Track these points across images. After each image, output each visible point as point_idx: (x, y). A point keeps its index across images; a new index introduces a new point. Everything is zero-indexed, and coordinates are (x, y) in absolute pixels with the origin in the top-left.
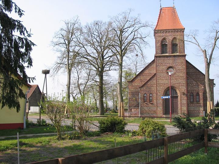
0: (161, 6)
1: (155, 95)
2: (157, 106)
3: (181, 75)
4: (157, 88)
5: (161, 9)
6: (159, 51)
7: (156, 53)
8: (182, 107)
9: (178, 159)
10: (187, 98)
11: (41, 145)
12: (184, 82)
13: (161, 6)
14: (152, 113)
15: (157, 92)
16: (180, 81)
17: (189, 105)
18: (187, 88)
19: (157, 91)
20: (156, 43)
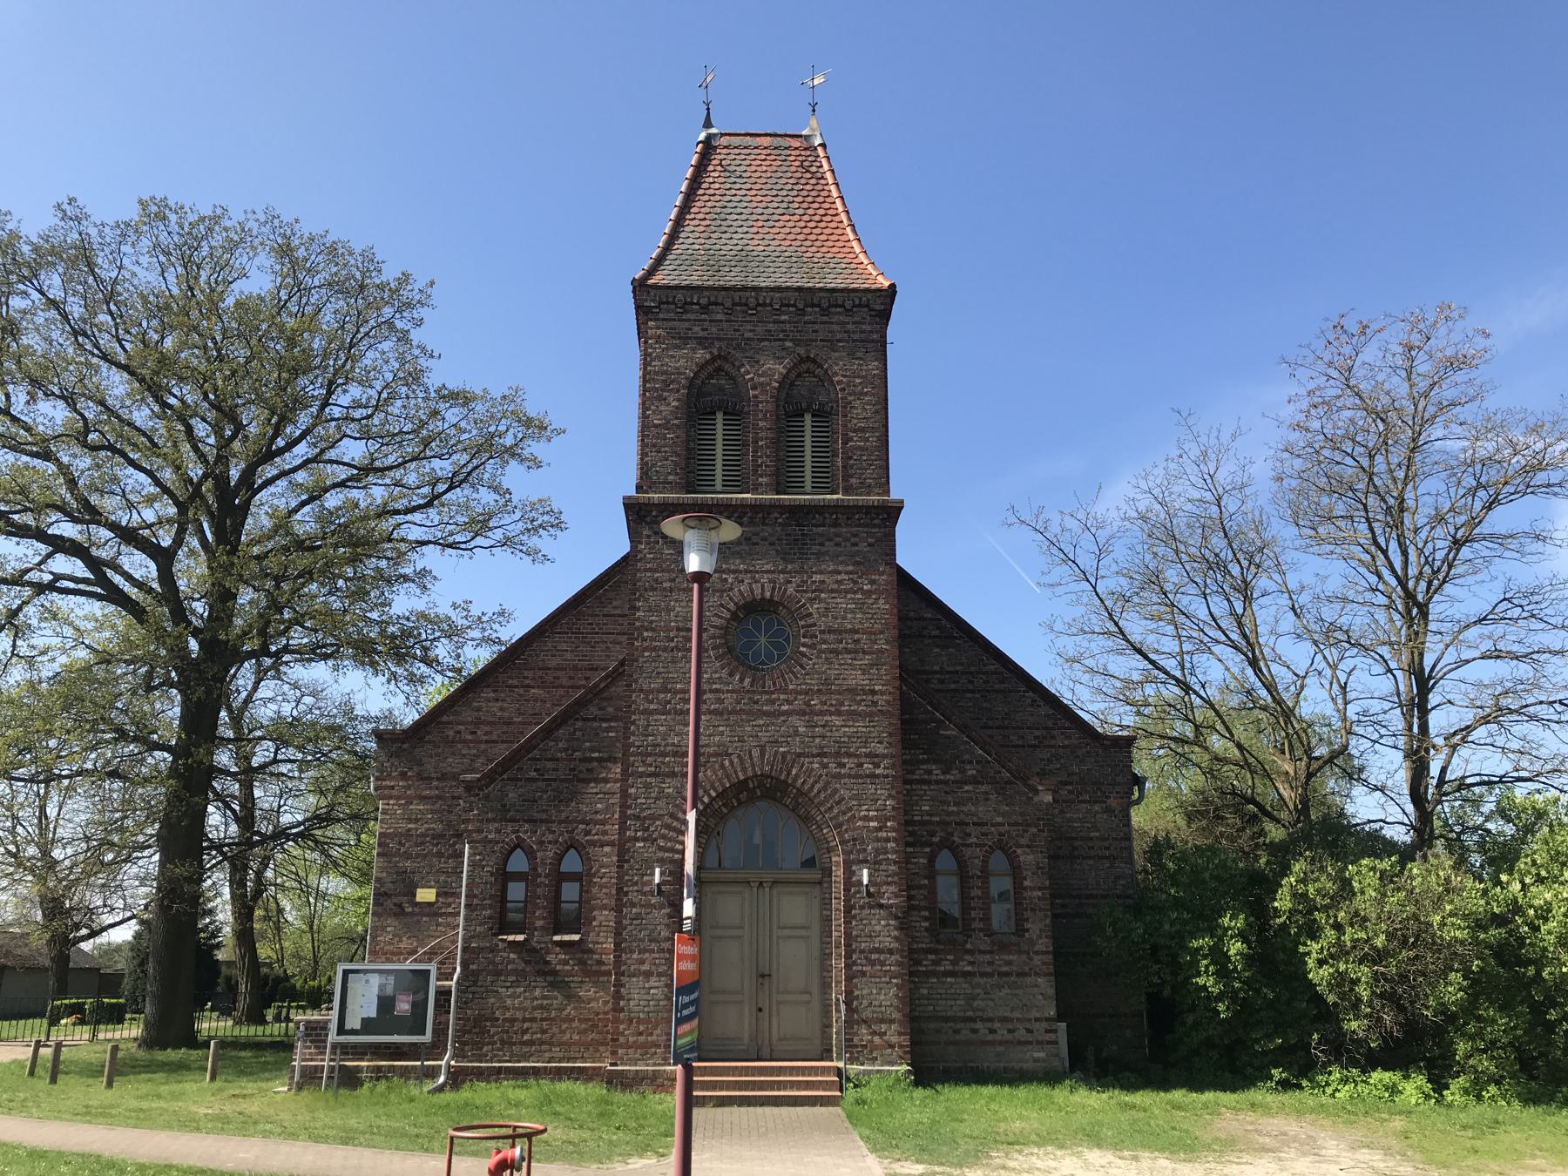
0: (708, 124)
1: (607, 856)
2: (620, 974)
3: (856, 678)
4: (624, 794)
5: (708, 147)
6: (666, 467)
7: (646, 480)
8: (863, 989)
9: (141, 1026)
10: (910, 898)
11: (691, 900)
12: (879, 738)
13: (708, 124)
14: (569, 1044)
15: (623, 828)
16: (841, 728)
17: (928, 960)
18: (906, 806)
19: (624, 818)
20: (652, 387)
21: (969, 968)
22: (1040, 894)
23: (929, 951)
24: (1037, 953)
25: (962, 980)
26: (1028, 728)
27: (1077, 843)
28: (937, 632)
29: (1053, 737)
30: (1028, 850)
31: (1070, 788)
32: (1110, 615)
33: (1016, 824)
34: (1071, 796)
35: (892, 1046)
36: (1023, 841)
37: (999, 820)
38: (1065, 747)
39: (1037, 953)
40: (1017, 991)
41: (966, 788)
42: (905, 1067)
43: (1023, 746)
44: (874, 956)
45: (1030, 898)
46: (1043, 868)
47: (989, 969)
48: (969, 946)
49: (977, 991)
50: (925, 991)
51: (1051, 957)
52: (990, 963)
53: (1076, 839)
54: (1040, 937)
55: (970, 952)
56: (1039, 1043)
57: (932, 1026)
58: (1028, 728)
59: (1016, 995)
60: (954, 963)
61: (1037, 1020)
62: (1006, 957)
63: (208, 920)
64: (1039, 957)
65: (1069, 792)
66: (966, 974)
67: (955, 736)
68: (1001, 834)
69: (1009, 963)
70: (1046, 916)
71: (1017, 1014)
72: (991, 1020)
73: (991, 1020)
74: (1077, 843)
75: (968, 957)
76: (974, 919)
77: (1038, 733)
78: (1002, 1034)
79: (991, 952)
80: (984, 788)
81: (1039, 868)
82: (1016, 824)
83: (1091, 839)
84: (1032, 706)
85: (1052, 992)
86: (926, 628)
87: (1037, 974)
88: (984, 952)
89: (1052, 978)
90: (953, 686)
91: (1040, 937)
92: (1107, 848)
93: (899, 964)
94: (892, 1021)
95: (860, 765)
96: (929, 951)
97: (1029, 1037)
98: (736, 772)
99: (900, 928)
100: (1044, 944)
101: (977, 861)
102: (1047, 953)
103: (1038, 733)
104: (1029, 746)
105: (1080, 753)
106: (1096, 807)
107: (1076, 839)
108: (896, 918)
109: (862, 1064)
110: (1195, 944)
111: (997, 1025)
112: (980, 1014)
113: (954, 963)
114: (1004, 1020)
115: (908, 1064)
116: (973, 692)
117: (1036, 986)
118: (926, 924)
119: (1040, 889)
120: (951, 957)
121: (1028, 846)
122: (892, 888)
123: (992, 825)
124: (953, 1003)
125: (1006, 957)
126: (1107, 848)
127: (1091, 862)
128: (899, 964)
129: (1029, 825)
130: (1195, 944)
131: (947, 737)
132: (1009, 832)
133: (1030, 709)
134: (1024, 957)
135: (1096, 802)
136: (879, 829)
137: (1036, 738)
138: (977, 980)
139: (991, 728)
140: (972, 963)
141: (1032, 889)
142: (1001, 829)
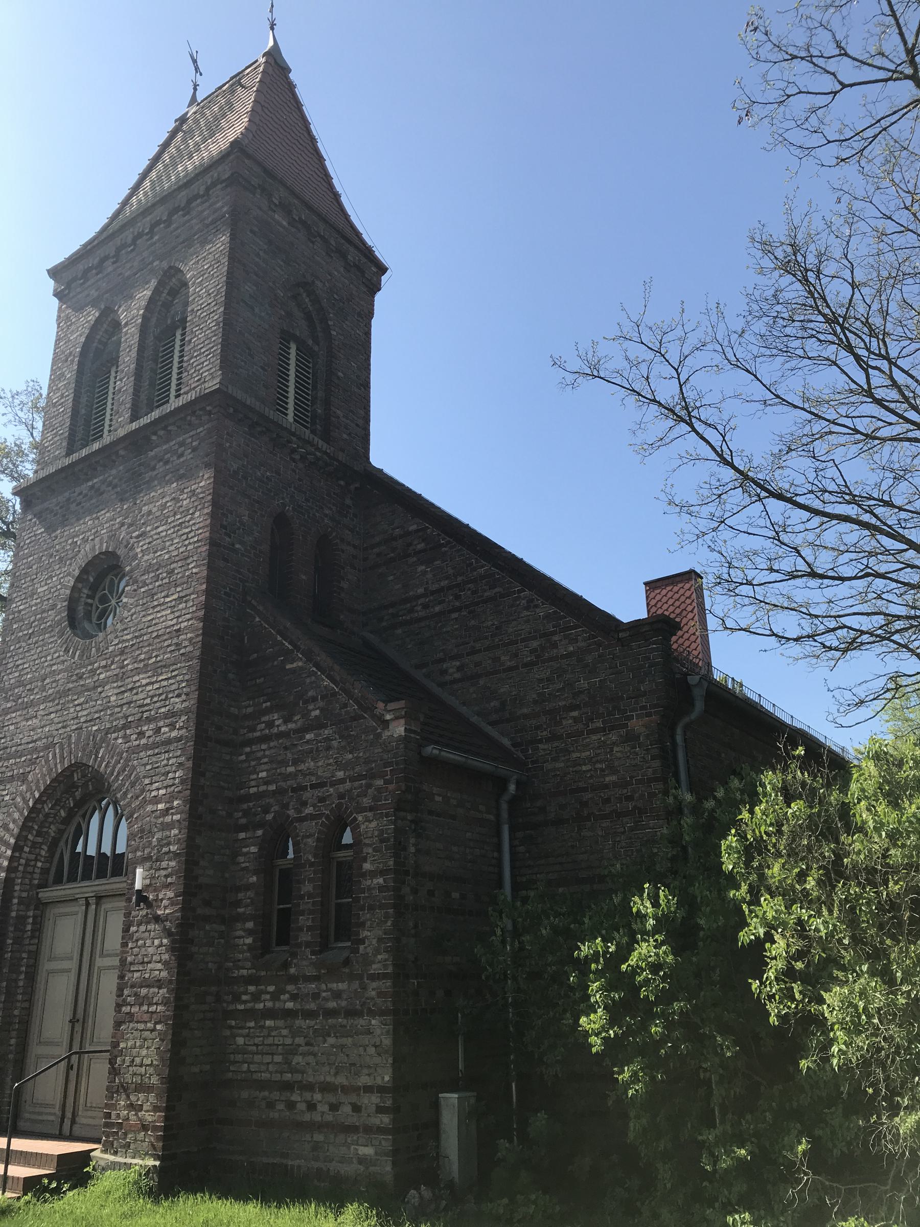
21: (290, 1005)
22: (381, 880)
23: (250, 980)
24: (373, 977)
25: (280, 1023)
26: (523, 640)
27: (587, 796)
28: (421, 546)
29: (554, 645)
30: (370, 814)
31: (575, 714)
32: (720, 456)
33: (360, 777)
34: (580, 726)
35: (145, 1128)
36: (366, 801)
37: (340, 774)
38: (569, 655)
39: (373, 977)
40: (344, 1041)
41: (308, 737)
42: (151, 1162)
43: (516, 668)
44: (144, 991)
45: (370, 889)
46: (387, 840)
47: (313, 1006)
48: (292, 971)
49: (298, 1040)
50: (240, 1041)
51: (389, 983)
52: (316, 996)
53: (585, 790)
54: (377, 951)
55: (294, 979)
56: (368, 1130)
57: (245, 1094)
58: (523, 640)
59: (342, 1046)
60: (275, 997)
61: (368, 1089)
62: (334, 986)
63: (915, 992)
64: (374, 984)
65: (575, 719)
66: (289, 1014)
67: (301, 668)
68: (341, 796)
69: (337, 995)
70: (387, 916)
71: (341, 1080)
72: (310, 1087)
73: (310, 1087)
74: (587, 796)
75: (290, 988)
76: (301, 929)
77: (535, 644)
78: (322, 1112)
79: (317, 978)
80: (327, 732)
81: (382, 841)
82: (360, 777)
83: (606, 786)
84: (527, 608)
85: (387, 1042)
86: (410, 544)
87: (372, 1013)
88: (308, 979)
89: (389, 1019)
90: (437, 609)
91: (377, 951)
92: (629, 798)
93: (165, 1002)
94: (148, 1089)
95: (158, 730)
96: (250, 980)
97: (354, 1120)
98: (56, 765)
99: (172, 949)
100: (381, 963)
101: (310, 841)
102: (385, 976)
103: (535, 644)
104: (526, 665)
105: (589, 659)
106: (613, 737)
107: (585, 790)
108: (169, 934)
109: (115, 1153)
110: (585, 950)
111: (318, 1096)
112: (298, 1077)
113: (275, 997)
114: (326, 1088)
115: (156, 1157)
116: (459, 609)
117: (369, 1032)
118: (249, 941)
119: (382, 873)
120: (271, 988)
121: (371, 809)
122: (170, 894)
123: (333, 784)
124: (267, 1059)
125: (334, 986)
126: (629, 798)
127: (606, 823)
128: (165, 1002)
129: (373, 777)
130: (585, 950)
131: (293, 671)
132: (350, 791)
133: (526, 613)
134: (356, 985)
135: (612, 728)
136: (166, 812)
137: (532, 651)
138: (299, 1022)
139: (480, 651)
140: (294, 997)
141: (373, 874)
142: (342, 788)
